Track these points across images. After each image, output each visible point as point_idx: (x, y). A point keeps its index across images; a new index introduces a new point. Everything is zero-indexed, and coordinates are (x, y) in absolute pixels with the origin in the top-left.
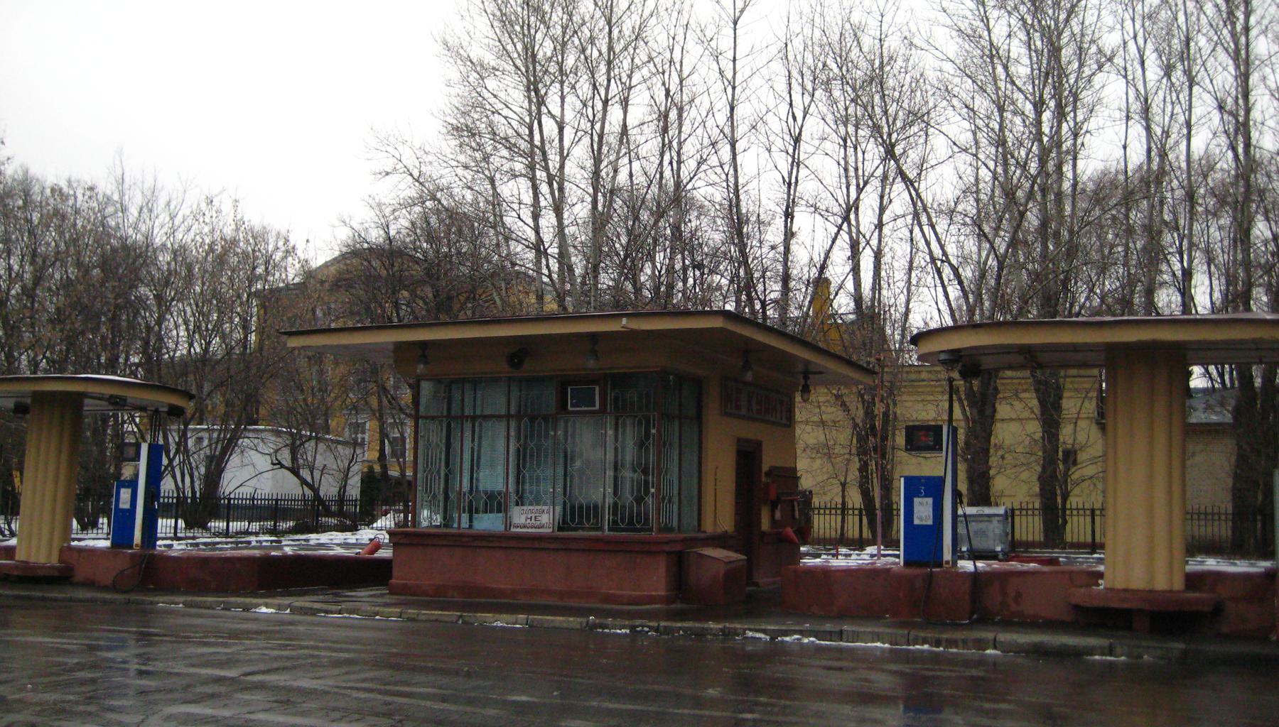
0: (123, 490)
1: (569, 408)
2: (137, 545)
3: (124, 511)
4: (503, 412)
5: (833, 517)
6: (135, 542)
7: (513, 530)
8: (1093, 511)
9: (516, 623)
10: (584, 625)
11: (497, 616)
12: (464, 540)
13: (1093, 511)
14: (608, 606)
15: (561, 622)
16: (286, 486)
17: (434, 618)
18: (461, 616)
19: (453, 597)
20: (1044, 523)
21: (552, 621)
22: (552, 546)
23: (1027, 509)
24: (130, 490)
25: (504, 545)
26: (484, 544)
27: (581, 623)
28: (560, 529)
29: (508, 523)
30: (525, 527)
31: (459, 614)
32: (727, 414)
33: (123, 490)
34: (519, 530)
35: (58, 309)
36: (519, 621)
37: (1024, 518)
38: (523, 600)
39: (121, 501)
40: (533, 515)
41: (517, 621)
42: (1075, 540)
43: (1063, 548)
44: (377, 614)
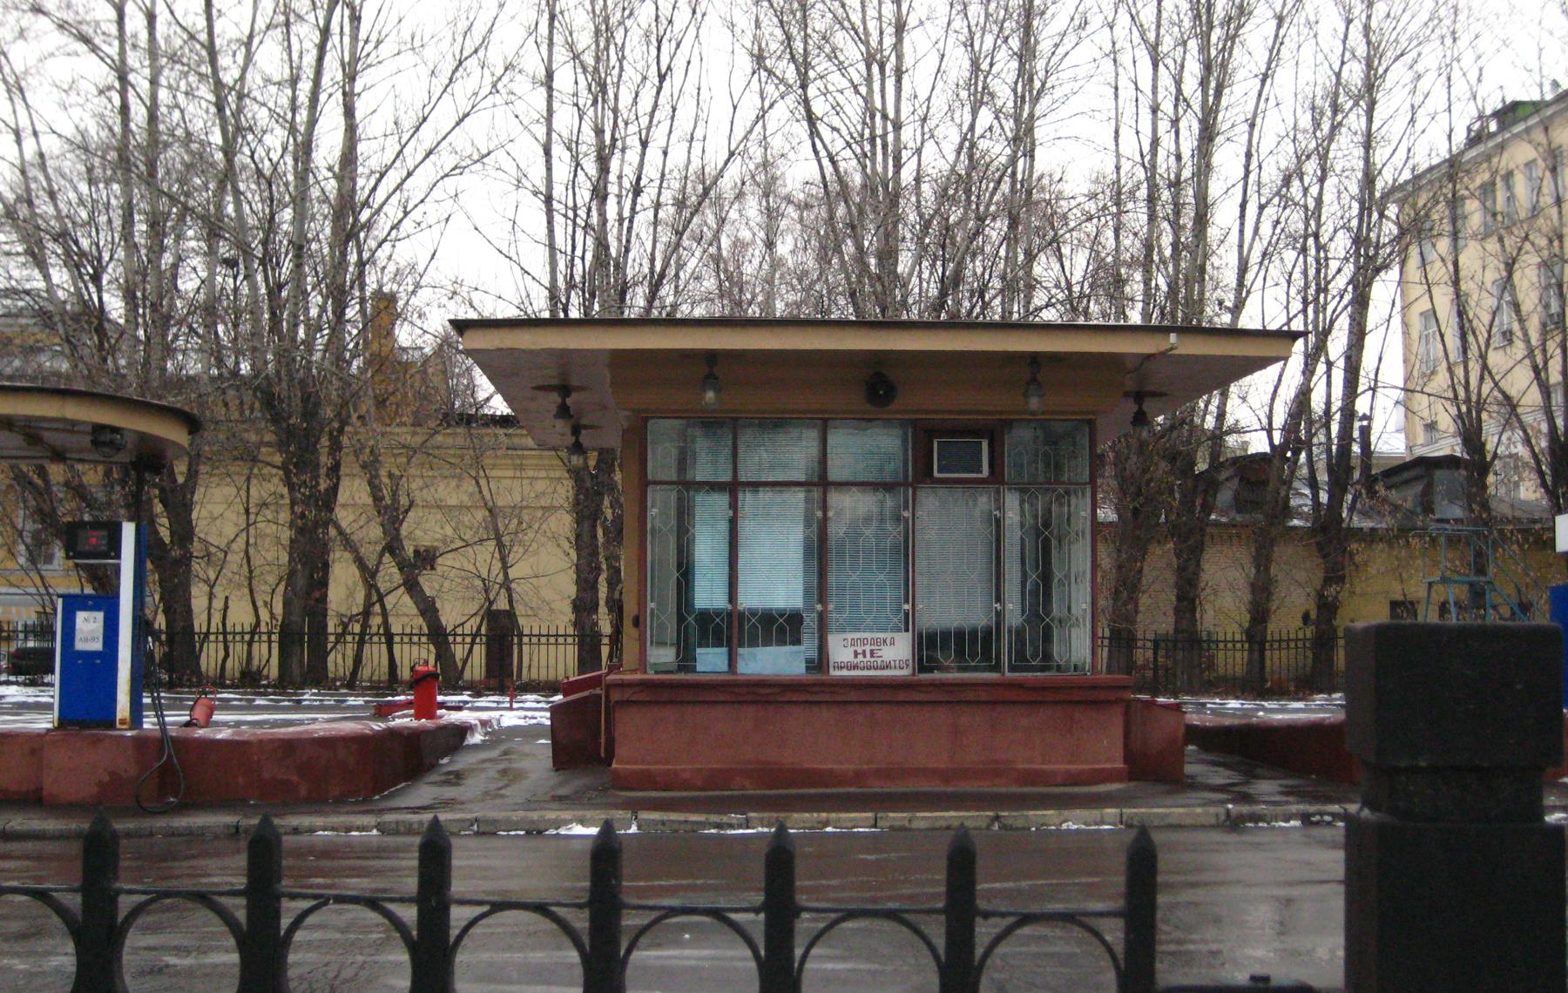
0: (81, 616)
1: (936, 474)
2: (123, 722)
3: (89, 655)
4: (726, 477)
5: (561, 648)
6: (119, 716)
7: (835, 673)
9: (1103, 823)
10: (1223, 817)
11: (1066, 813)
12: (763, 691)
14: (1026, 790)
15: (1180, 815)
16: (378, 605)
17: (944, 824)
18: (997, 818)
19: (743, 788)
20: (488, 654)
21: (1166, 815)
22: (932, 697)
24: (100, 615)
25: (839, 698)
26: (803, 697)
27: (1217, 815)
28: (922, 669)
29: (820, 662)
30: (855, 667)
31: (991, 814)
33: (81, 616)
34: (845, 673)
35: (45, 247)
36: (1107, 819)
37: (406, 647)
38: (876, 788)
39: (78, 636)
40: (868, 648)
41: (860, 823)
42: (543, 677)
43: (189, 687)
44: (826, 824)
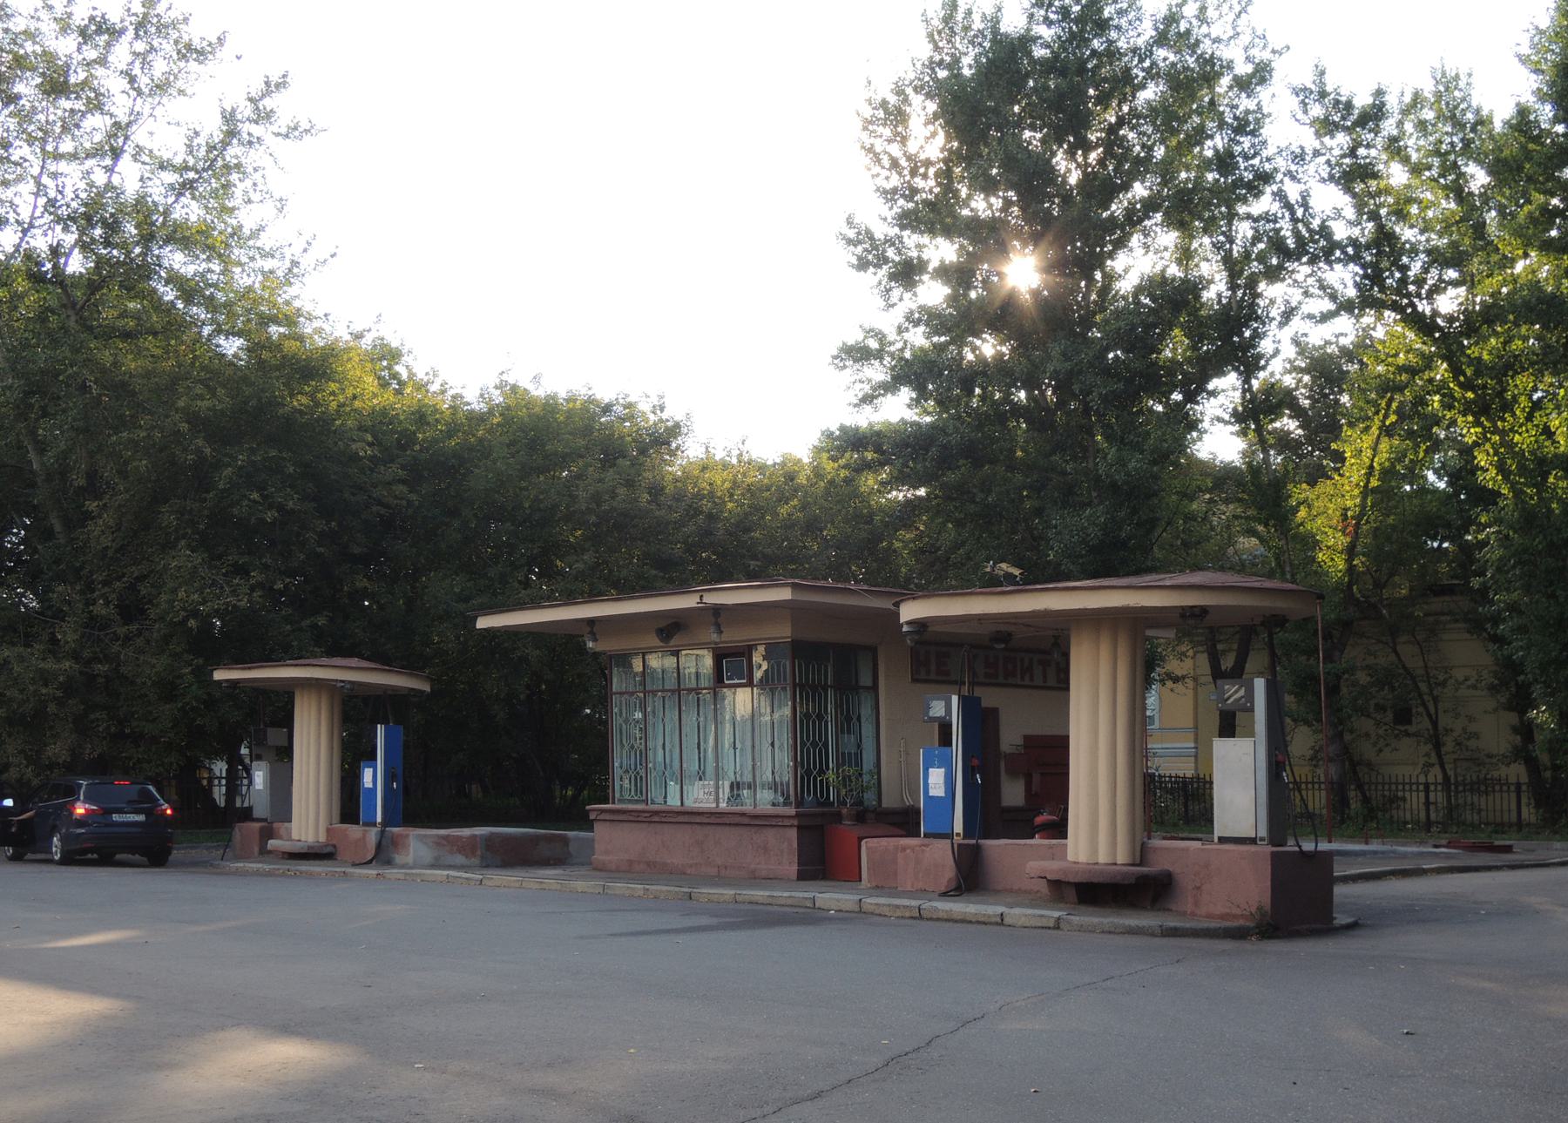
4: (682, 687)
23: (1313, 783)
32: (915, 680)
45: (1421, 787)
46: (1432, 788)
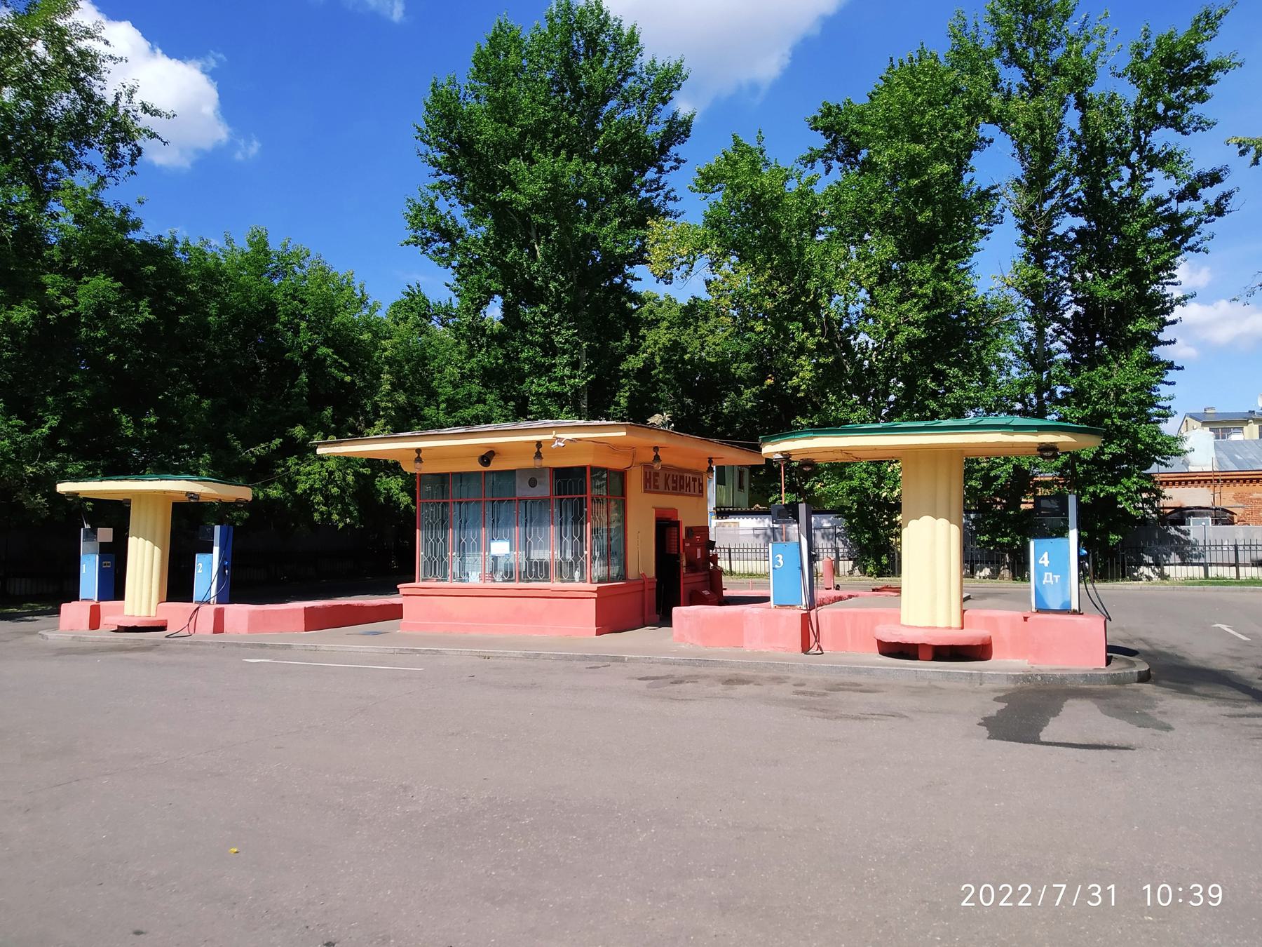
8: (730, 549)
13: (730, 549)
45: (727, 551)
46: (732, 551)
